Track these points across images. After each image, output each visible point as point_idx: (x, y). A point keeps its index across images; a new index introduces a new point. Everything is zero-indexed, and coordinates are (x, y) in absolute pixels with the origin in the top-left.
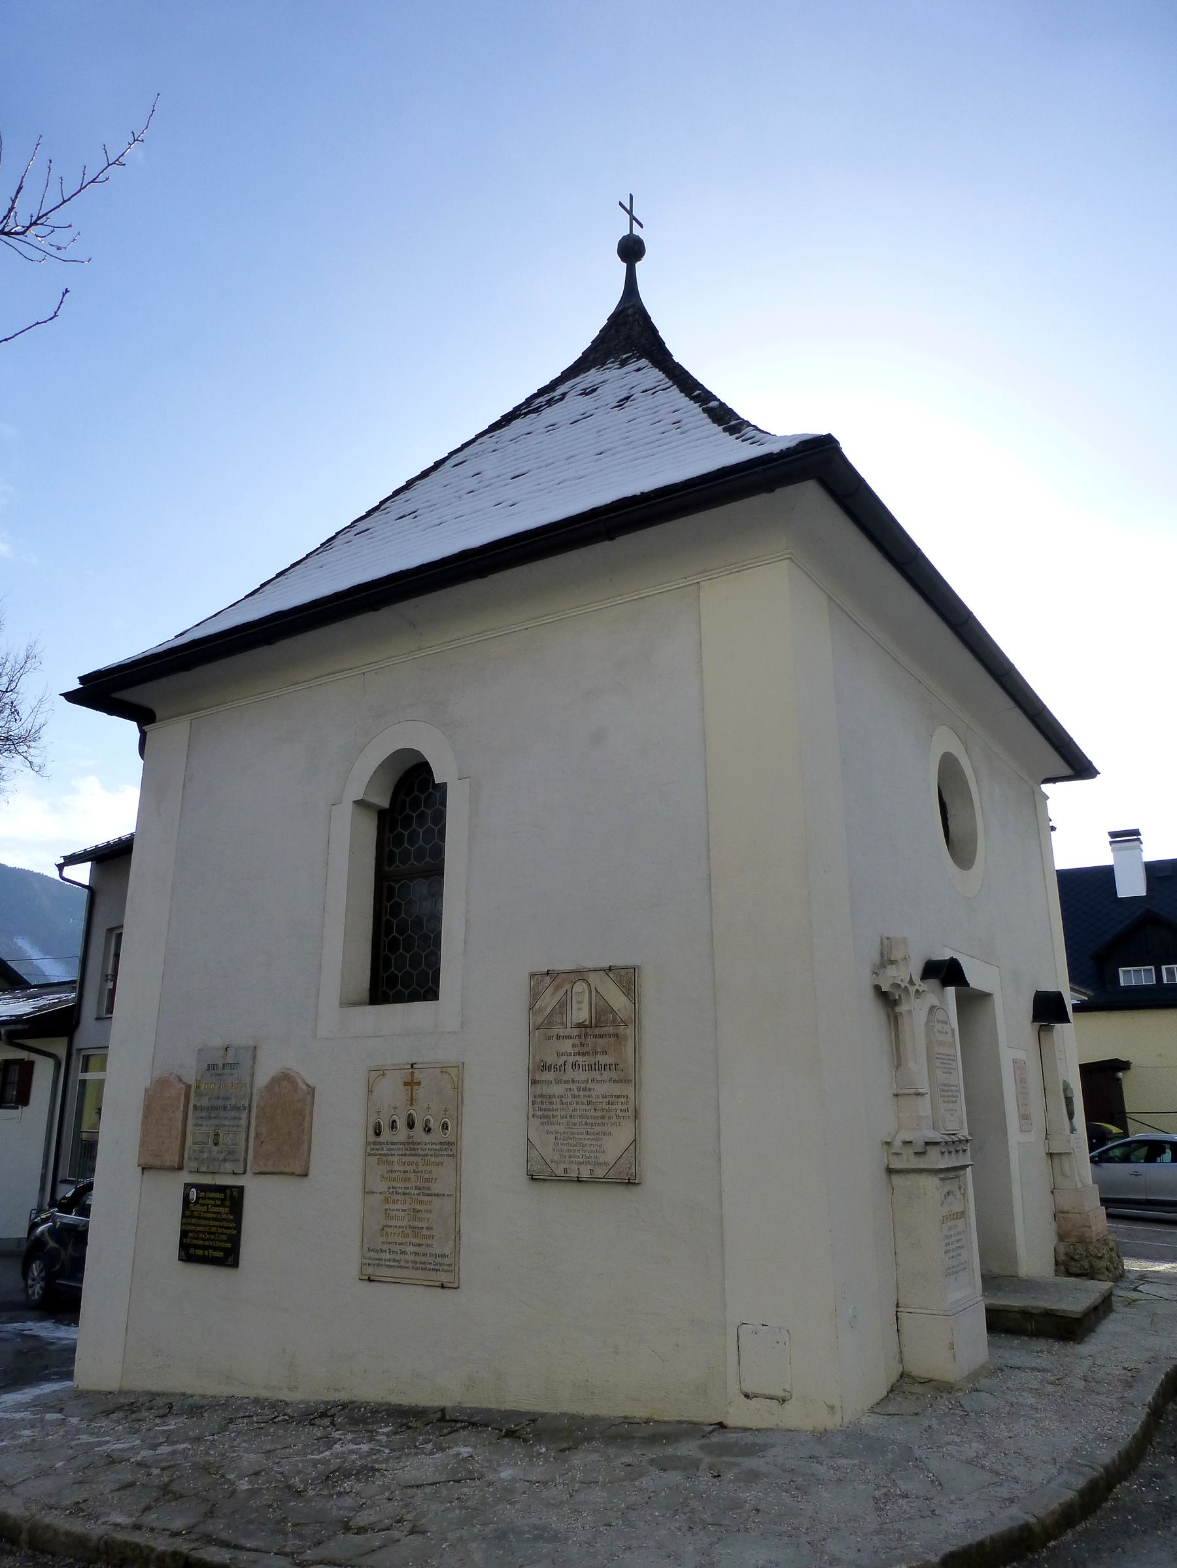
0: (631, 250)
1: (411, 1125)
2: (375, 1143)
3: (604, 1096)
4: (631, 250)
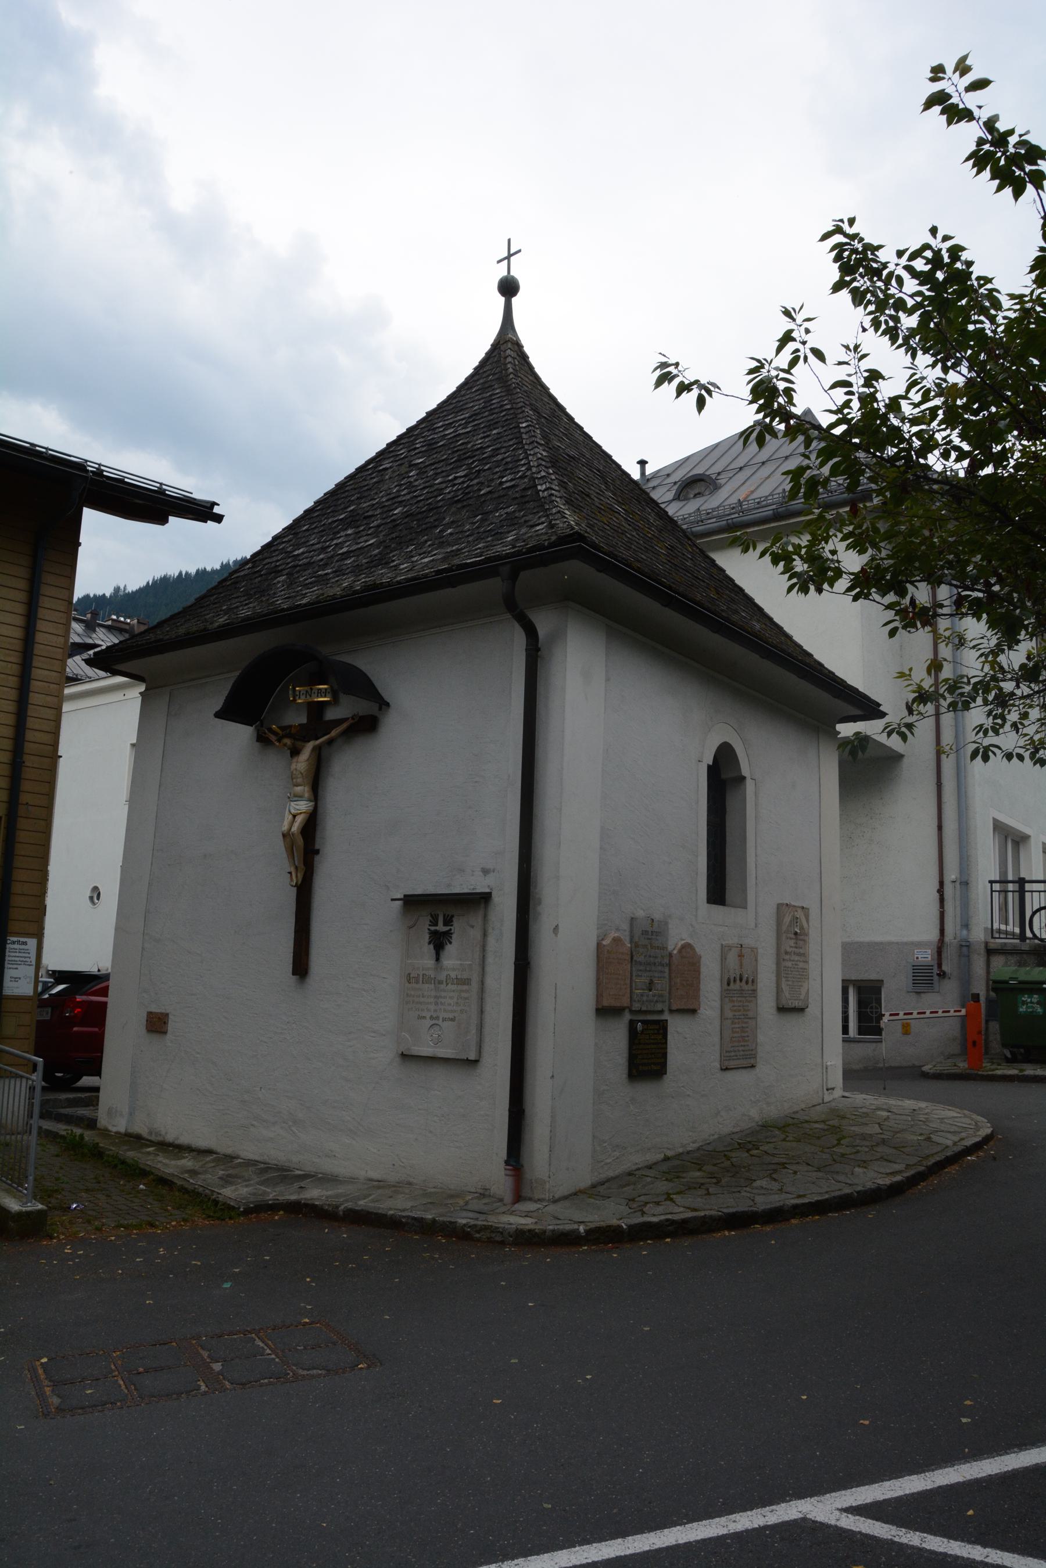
0: (509, 288)
1: (741, 980)
2: (728, 990)
3: (801, 969)
4: (509, 288)
